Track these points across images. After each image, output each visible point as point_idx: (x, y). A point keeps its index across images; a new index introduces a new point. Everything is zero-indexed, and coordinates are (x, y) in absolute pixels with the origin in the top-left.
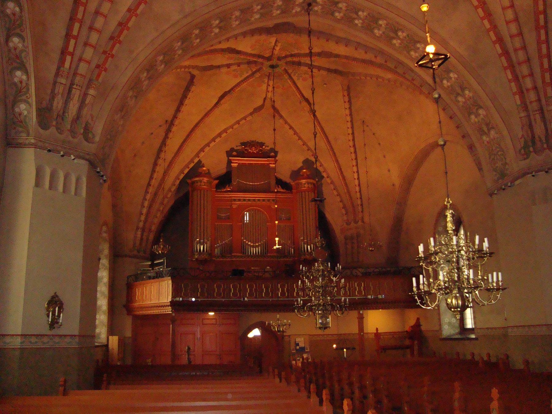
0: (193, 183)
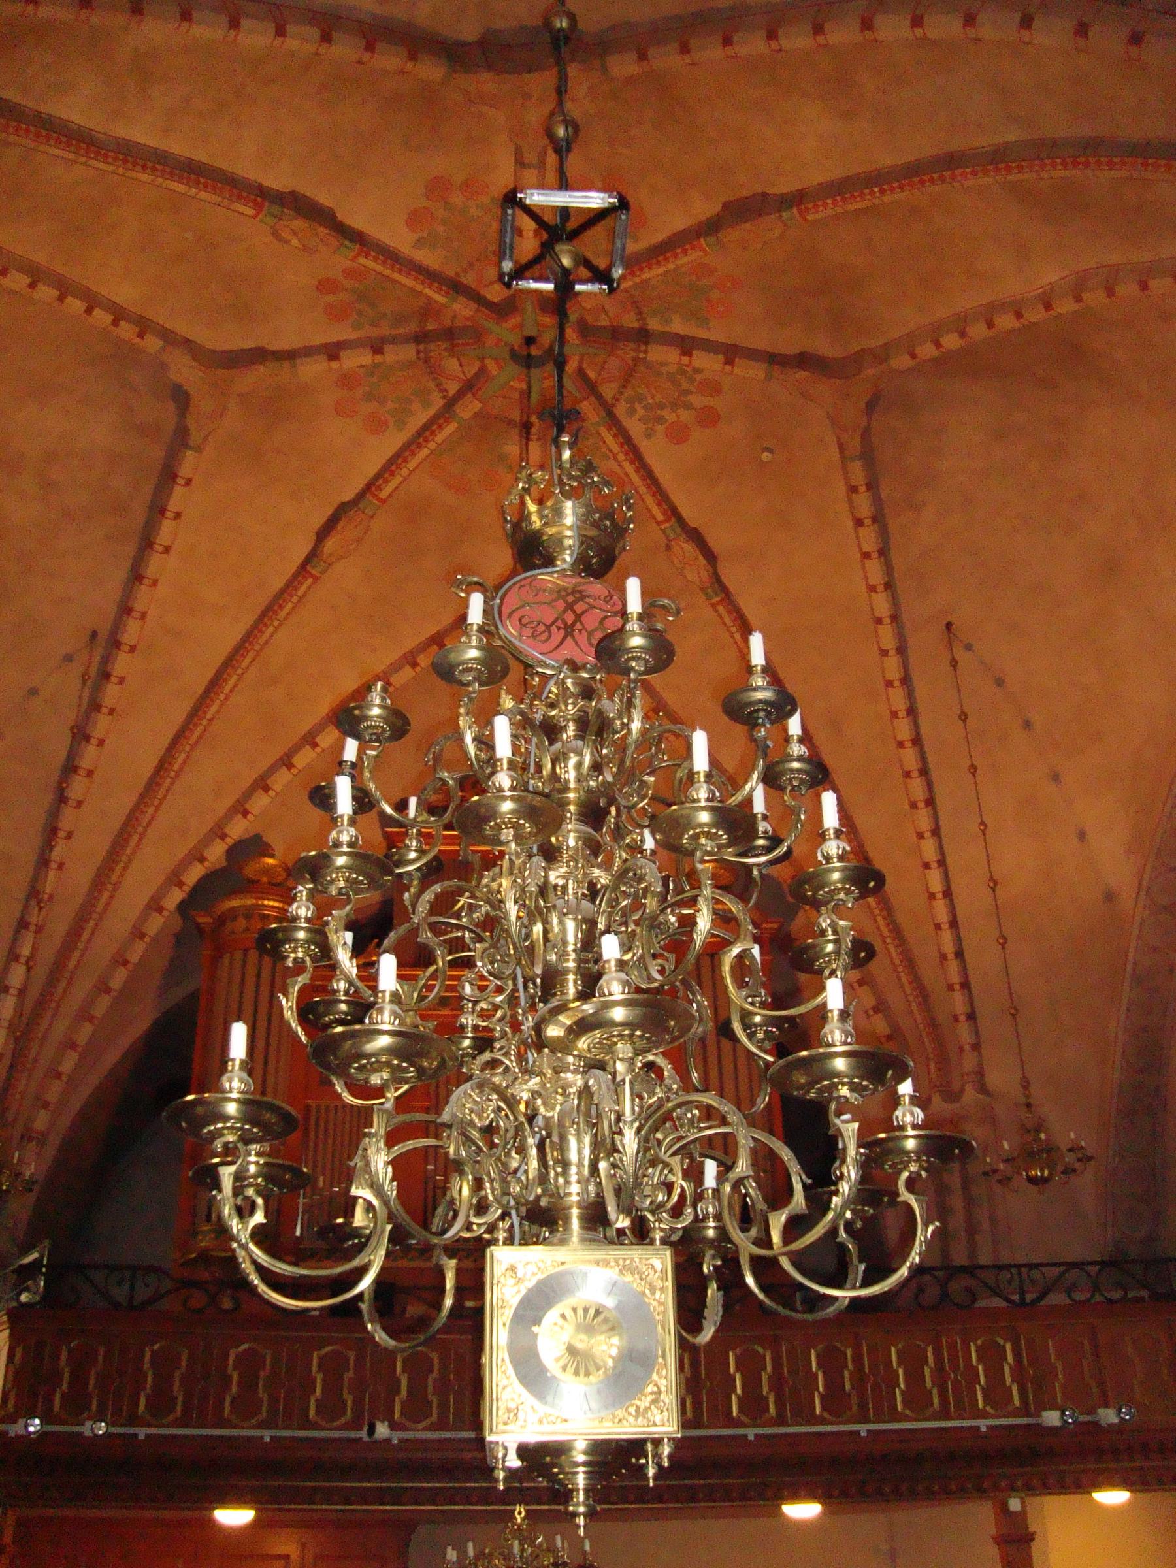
0: (222, 920)
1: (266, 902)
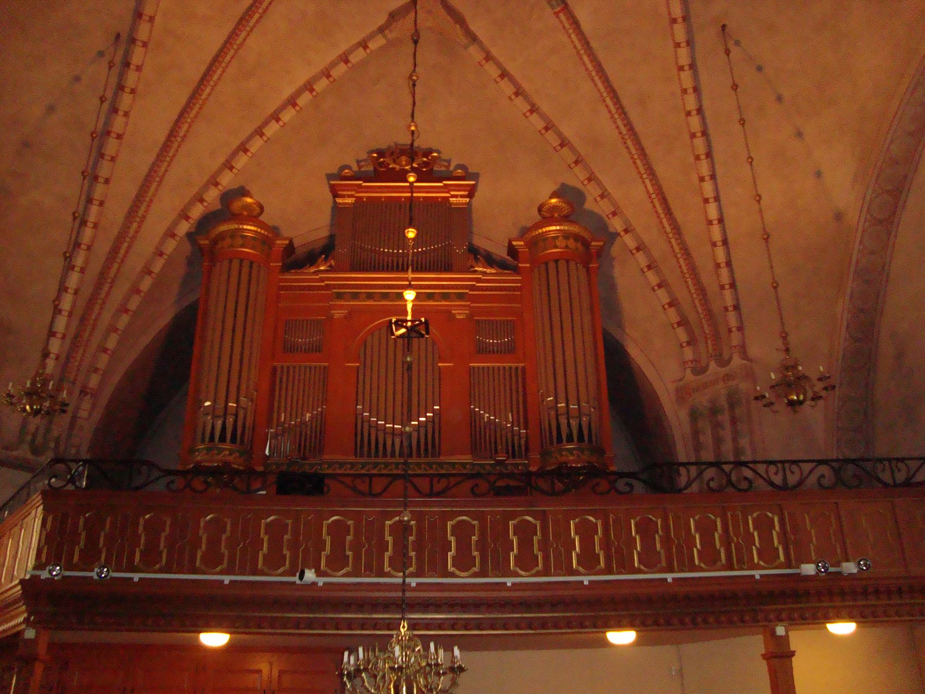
1: (245, 227)
